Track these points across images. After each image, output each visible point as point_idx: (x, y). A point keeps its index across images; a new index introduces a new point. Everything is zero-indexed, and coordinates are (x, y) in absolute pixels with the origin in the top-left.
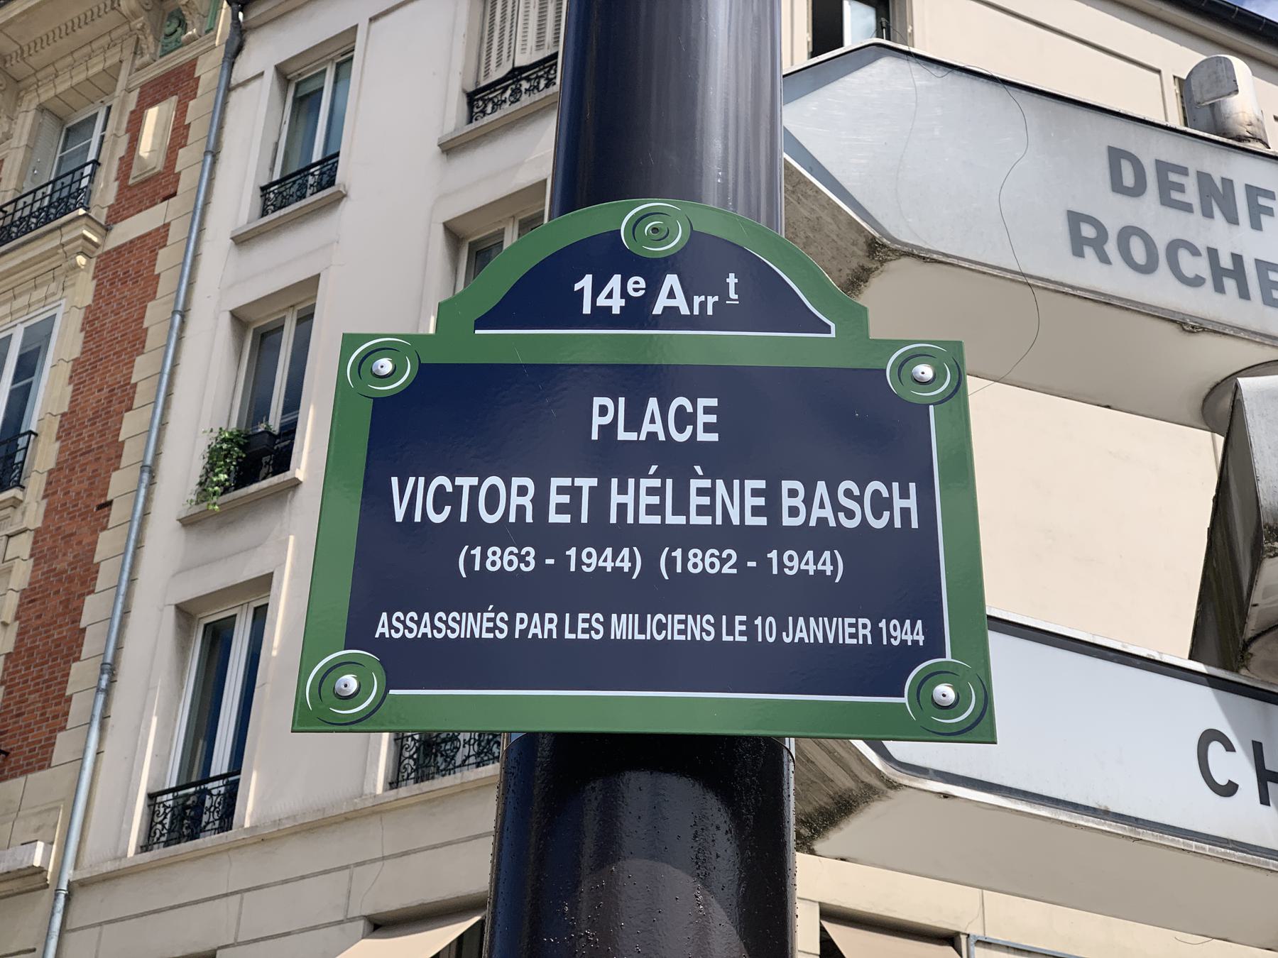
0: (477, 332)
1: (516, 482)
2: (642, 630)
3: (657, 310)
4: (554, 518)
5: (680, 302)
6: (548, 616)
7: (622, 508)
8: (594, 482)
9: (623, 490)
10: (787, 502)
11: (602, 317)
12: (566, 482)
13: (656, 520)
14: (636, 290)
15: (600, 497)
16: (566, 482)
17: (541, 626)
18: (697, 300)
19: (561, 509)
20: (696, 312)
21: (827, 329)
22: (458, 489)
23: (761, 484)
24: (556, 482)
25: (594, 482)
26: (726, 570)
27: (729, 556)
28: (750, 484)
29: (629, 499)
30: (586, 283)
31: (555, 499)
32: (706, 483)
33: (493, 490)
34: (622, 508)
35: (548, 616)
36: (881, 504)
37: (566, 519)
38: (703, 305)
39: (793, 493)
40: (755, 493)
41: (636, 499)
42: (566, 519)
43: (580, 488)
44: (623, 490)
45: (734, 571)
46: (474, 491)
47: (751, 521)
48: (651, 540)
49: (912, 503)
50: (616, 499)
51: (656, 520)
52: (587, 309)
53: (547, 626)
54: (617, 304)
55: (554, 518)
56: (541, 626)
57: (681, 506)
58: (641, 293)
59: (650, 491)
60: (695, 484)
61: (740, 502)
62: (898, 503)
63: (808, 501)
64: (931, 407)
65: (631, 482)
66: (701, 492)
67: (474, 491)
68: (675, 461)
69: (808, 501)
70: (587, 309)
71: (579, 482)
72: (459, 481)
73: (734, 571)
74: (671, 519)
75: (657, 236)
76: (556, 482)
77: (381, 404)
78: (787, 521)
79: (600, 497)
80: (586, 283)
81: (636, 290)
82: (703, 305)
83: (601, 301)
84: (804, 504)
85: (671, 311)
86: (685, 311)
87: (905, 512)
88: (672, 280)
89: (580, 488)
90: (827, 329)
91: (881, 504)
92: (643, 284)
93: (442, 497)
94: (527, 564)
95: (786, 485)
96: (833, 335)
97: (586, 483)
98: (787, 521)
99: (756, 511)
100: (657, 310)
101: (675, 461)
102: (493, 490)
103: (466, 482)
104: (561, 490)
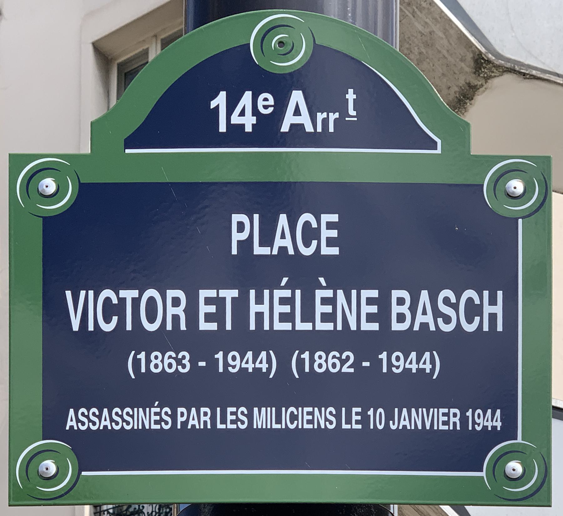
0: (127, 151)
1: (171, 294)
2: (279, 421)
3: (285, 128)
4: (204, 326)
5: (305, 119)
6: (203, 410)
7: (259, 316)
8: (235, 293)
9: (259, 300)
10: (396, 309)
11: (236, 135)
12: (212, 293)
13: (287, 326)
14: (266, 107)
15: (241, 305)
16: (212, 293)
17: (198, 418)
18: (320, 116)
19: (209, 318)
20: (202, 427)
21: (434, 145)
22: (122, 301)
23: (374, 293)
24: (203, 294)
25: (235, 293)
26: (345, 369)
27: (348, 358)
28: (366, 294)
29: (264, 308)
30: (220, 101)
31: (204, 309)
32: (329, 293)
33: (151, 301)
34: (259, 316)
35: (203, 410)
36: (473, 310)
37: (213, 326)
38: (325, 122)
39: (401, 301)
40: (370, 301)
41: (270, 308)
42: (213, 326)
43: (224, 299)
44: (259, 300)
45: (352, 370)
46: (136, 302)
47: (366, 326)
48: (284, 344)
49: (498, 309)
50: (254, 308)
51: (287, 326)
52: (223, 128)
53: (203, 418)
54: (249, 122)
55: (204, 326)
56: (198, 418)
57: (308, 316)
58: (270, 110)
59: (283, 301)
60: (320, 294)
61: (355, 310)
62: (487, 309)
63: (413, 309)
64: (520, 221)
65: (266, 292)
66: (325, 301)
67: (136, 302)
68: (302, 272)
69: (413, 309)
70: (223, 128)
71: (223, 293)
72: (123, 293)
73: (352, 370)
74: (301, 326)
75: (282, 50)
76: (203, 294)
77: (50, 223)
78: (396, 326)
79: (241, 305)
80: (220, 101)
81: (266, 107)
82: (325, 122)
83: (235, 119)
84: (410, 312)
85: (297, 128)
86: (309, 128)
87: (493, 317)
88: (297, 97)
89: (224, 299)
90: (434, 145)
91: (473, 310)
92: (271, 102)
93: (110, 310)
94: (184, 366)
95: (396, 294)
96: (439, 151)
97: (230, 294)
98: (396, 326)
99: (371, 318)
100: (285, 128)
101: (302, 272)
102: (151, 301)
103: (129, 294)
104: (208, 301)
